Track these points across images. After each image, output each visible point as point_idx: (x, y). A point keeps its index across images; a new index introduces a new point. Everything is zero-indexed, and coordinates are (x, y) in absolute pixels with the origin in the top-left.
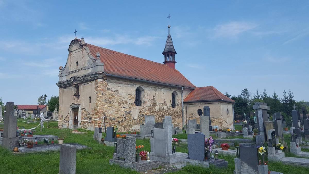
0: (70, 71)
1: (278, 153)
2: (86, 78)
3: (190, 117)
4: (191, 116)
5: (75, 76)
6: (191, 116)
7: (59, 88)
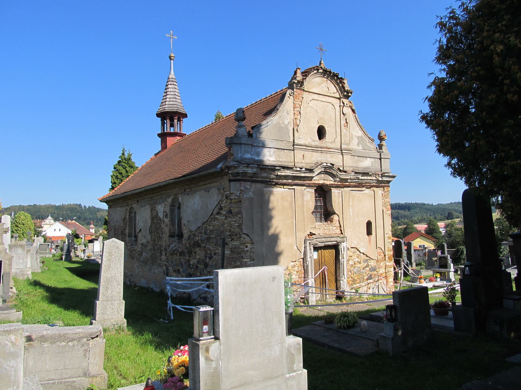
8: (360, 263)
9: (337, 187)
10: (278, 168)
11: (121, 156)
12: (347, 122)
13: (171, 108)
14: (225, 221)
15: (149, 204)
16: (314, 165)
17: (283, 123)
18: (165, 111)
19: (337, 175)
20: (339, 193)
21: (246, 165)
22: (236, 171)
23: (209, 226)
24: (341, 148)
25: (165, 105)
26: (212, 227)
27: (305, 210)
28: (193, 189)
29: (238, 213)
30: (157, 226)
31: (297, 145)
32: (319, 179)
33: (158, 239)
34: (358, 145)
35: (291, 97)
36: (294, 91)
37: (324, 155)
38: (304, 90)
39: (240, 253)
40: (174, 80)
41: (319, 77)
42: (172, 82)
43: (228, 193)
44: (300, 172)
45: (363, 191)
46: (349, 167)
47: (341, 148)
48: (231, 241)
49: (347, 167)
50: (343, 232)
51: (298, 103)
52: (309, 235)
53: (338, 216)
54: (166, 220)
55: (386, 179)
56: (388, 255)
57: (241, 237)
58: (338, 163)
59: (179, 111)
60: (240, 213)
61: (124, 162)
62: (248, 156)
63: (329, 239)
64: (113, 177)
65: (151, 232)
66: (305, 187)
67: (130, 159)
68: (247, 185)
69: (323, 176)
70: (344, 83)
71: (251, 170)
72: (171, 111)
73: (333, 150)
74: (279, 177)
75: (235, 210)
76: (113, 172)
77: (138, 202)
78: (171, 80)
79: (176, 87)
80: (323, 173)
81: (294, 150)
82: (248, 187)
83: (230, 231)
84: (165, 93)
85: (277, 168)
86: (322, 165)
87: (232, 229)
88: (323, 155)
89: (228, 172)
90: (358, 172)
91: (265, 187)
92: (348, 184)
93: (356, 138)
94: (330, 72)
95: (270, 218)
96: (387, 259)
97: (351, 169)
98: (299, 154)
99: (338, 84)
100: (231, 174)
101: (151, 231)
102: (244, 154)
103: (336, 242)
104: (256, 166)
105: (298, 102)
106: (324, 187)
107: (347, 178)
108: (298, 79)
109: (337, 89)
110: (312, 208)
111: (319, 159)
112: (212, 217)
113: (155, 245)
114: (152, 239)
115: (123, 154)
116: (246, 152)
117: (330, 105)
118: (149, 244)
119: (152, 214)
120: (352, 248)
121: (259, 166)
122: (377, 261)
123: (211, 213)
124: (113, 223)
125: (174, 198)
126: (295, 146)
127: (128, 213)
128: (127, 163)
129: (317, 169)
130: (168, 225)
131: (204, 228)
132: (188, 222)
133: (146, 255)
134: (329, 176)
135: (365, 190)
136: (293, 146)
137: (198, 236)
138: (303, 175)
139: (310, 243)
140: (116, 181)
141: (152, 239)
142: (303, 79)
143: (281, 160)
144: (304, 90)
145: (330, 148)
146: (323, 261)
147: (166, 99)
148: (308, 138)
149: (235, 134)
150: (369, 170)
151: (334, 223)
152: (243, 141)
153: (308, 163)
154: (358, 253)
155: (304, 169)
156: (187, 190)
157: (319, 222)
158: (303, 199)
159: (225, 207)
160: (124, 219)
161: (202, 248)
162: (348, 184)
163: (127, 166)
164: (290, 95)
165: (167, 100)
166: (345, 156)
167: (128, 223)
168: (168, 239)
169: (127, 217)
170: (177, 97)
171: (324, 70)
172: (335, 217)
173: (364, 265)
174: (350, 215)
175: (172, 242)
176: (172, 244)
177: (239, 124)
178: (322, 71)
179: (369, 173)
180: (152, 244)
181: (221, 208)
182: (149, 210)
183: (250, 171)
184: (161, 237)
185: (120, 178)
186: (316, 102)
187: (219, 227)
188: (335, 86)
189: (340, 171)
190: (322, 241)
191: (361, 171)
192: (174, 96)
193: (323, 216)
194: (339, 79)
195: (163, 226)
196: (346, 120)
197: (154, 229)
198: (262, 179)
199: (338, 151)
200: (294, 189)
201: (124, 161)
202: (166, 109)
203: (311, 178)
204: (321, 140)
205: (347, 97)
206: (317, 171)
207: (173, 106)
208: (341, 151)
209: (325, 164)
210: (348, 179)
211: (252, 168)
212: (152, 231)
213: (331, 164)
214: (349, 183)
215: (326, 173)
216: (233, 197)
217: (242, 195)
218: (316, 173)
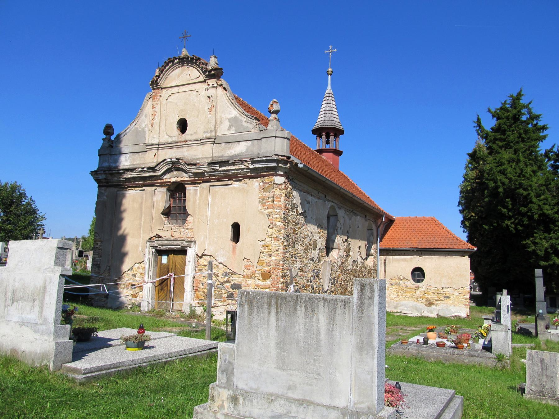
0: (151, 142)
1: (118, 306)
2: (221, 169)
3: (392, 285)
4: (394, 282)
5: (178, 159)
6: (394, 282)
7: (99, 187)
9: (192, 183)
10: (122, 171)
32: (173, 178)
37: (180, 150)
38: (162, 88)
40: (331, 95)
44: (144, 172)
45: (230, 185)
46: (206, 158)
49: (204, 159)
55: (260, 166)
58: (196, 155)
59: (326, 126)
63: (171, 243)
71: (100, 176)
74: (128, 179)
82: (103, 192)
85: (120, 171)
86: (165, 161)
95: (121, 220)
103: (180, 247)
104: (103, 172)
109: (200, 72)
121: (105, 172)
134: (183, 172)
138: (147, 175)
145: (187, 141)
174: (207, 216)
179: (228, 161)
186: (177, 95)
188: (198, 70)
190: (162, 244)
213: (176, 159)
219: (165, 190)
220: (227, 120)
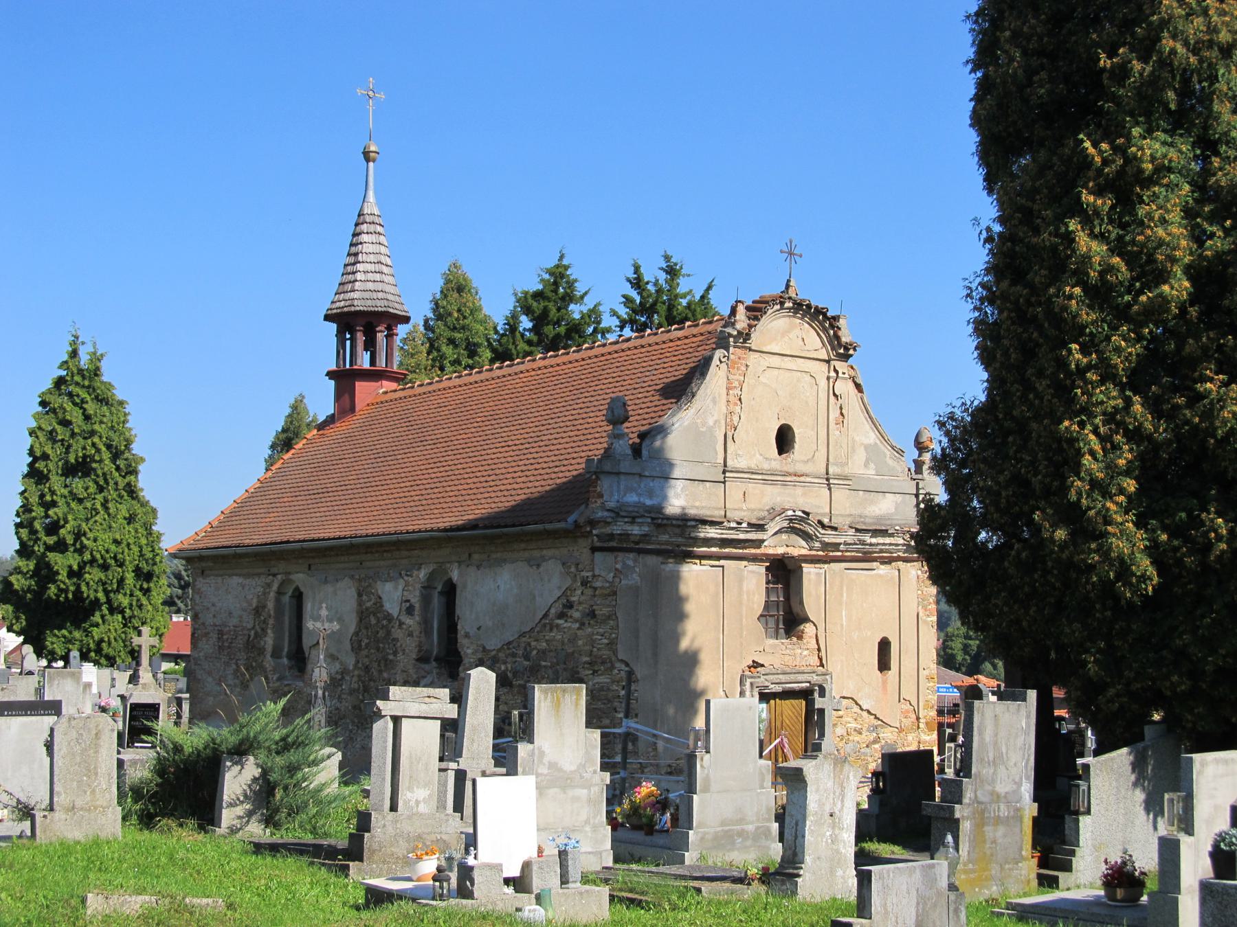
8: (860, 733)
10: (693, 523)
11: (66, 362)
12: (842, 414)
13: (369, 303)
14: (580, 633)
15: (352, 577)
16: (766, 513)
17: (704, 424)
18: (353, 309)
19: (816, 535)
20: (818, 574)
21: (630, 520)
22: (608, 530)
23: (537, 640)
24: (827, 474)
25: (354, 291)
26: (544, 644)
27: (744, 613)
28: (494, 556)
29: (609, 617)
30: (378, 633)
31: (732, 472)
32: (776, 545)
33: (379, 665)
34: (866, 465)
35: (724, 366)
36: (728, 353)
37: (789, 490)
38: (750, 350)
39: (609, 701)
40: (377, 220)
41: (784, 316)
42: (372, 226)
43: (589, 574)
46: (842, 516)
47: (827, 474)
48: (593, 674)
50: (824, 662)
51: (736, 377)
52: (749, 667)
53: (815, 625)
54: (408, 621)
56: (925, 717)
57: (613, 667)
58: (819, 507)
60: (612, 616)
61: (77, 384)
62: (632, 498)
63: (793, 677)
64: (39, 433)
65: (356, 647)
66: (745, 563)
67: (96, 372)
68: (628, 558)
69: (784, 536)
70: (840, 329)
71: (637, 528)
72: (369, 309)
73: (808, 479)
75: (602, 611)
76: (37, 417)
77: (309, 569)
78: (368, 219)
79: (382, 239)
80: (786, 532)
81: (724, 482)
82: (630, 563)
83: (591, 655)
84: (349, 255)
87: (595, 649)
88: (787, 491)
89: (591, 532)
90: (864, 527)
91: (662, 563)
92: (840, 554)
93: (862, 448)
94: (809, 306)
96: (921, 725)
97: (848, 521)
98: (735, 489)
99: (825, 330)
100: (597, 535)
101: (355, 645)
102: (625, 495)
104: (649, 520)
105: (737, 377)
106: (786, 561)
107: (838, 541)
108: (739, 326)
110: (759, 609)
111: (778, 499)
112: (546, 623)
113: (370, 680)
114: (360, 665)
115: (74, 354)
116: (630, 489)
117: (807, 378)
118: (347, 678)
119: (360, 604)
120: (844, 698)
122: (901, 730)
123: (544, 612)
124: (214, 616)
125: (434, 570)
126: (728, 474)
127: (272, 595)
128: (89, 387)
129: (772, 524)
130: (416, 633)
131: (523, 645)
132: (479, 629)
133: (338, 705)
135: (878, 568)
136: (724, 472)
137: (505, 663)
138: (742, 536)
139: (752, 684)
140: (50, 452)
141: (360, 665)
142: (750, 326)
143: (697, 504)
144: (750, 350)
145: (802, 475)
146: (778, 724)
147: (354, 273)
148: (754, 455)
149: (606, 450)
150: (888, 522)
151: (805, 641)
152: (625, 466)
153: (753, 510)
154: (856, 709)
155: (744, 525)
156: (476, 556)
157: (771, 637)
158: (740, 587)
159: (580, 603)
160: (258, 611)
161: (516, 690)
162: (840, 554)
163: (88, 398)
164: (721, 362)
165: (359, 276)
166: (837, 493)
167: (271, 621)
168: (415, 665)
169: (271, 605)
170: (385, 269)
171: (795, 303)
172: (808, 629)
173: (868, 737)
174: (842, 625)
175: (423, 673)
176: (424, 677)
177: (616, 432)
178: (791, 305)
180: (359, 676)
181: (570, 605)
182: (352, 592)
183: (636, 530)
184: (391, 661)
185: (62, 440)
186: (776, 372)
187: (563, 643)
188: (818, 334)
189: (823, 526)
190: (778, 681)
191: (871, 524)
192: (378, 267)
193: (781, 626)
194: (829, 319)
195: (397, 633)
196: (841, 408)
197: (366, 641)
198: (658, 547)
199: (820, 481)
200: (723, 567)
201: (77, 378)
202: (356, 303)
203: (758, 543)
204: (784, 455)
205: (845, 357)
206: (773, 527)
207: (375, 295)
208: (828, 479)
209: (790, 513)
210: (840, 544)
211: (641, 524)
212: (360, 646)
213: (804, 512)
214: (842, 551)
215: (792, 530)
216: (598, 584)
217: (617, 580)
218: (771, 532)
219: (763, 570)
220: (862, 448)
